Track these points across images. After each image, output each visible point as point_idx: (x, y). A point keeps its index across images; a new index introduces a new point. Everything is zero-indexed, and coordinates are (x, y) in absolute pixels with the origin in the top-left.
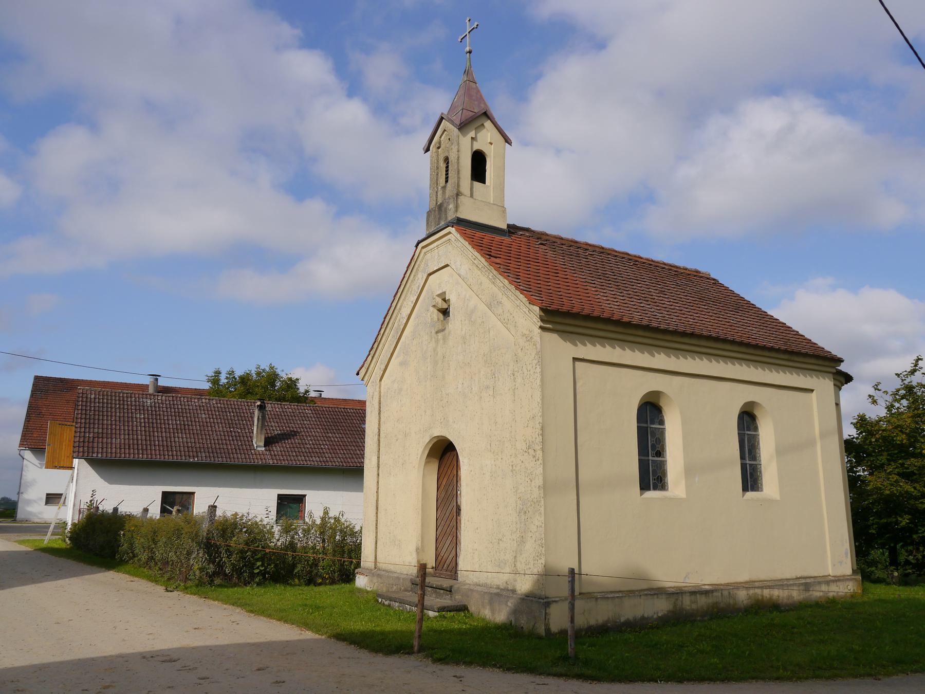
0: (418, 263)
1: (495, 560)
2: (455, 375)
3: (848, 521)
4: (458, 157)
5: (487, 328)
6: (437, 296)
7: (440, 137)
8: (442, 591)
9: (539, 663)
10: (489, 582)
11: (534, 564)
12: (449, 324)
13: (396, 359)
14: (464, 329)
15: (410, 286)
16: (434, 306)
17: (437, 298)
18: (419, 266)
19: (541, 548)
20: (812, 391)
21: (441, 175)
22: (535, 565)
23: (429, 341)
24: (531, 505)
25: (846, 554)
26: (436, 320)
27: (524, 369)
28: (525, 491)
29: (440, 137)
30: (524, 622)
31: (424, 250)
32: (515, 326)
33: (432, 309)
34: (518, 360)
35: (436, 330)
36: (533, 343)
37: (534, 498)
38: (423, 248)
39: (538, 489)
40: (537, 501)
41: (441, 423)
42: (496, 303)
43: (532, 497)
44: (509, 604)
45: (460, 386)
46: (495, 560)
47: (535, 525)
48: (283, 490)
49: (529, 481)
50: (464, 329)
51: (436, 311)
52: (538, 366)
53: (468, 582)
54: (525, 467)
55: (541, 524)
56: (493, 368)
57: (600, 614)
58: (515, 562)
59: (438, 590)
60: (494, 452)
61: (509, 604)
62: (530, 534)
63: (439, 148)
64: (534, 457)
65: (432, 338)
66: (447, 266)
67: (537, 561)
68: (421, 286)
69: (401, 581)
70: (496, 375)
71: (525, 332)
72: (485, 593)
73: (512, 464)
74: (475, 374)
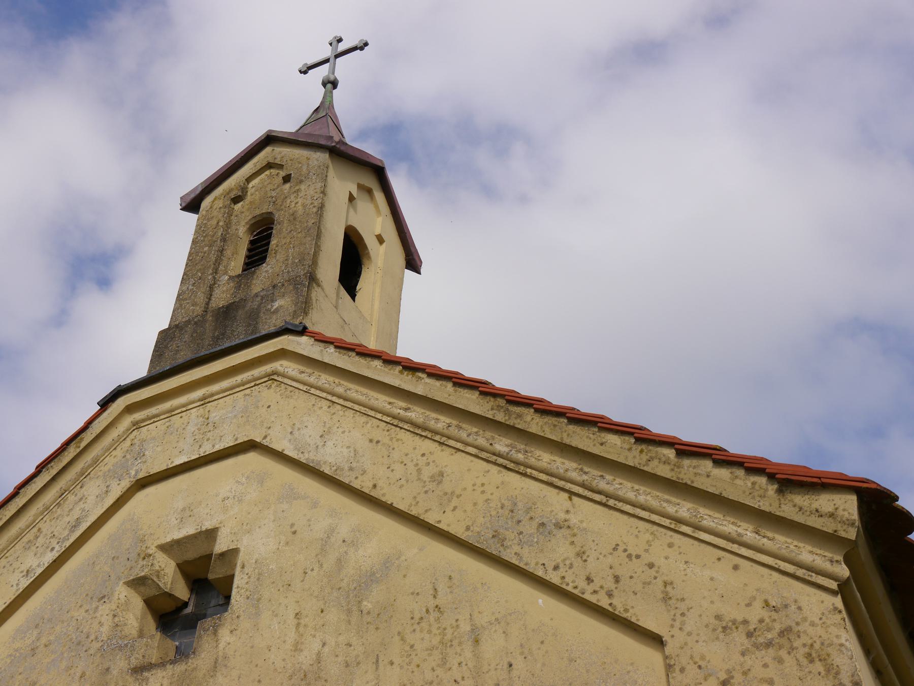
0: (88, 457)
3: (257, 140)
4: (322, 207)
5: (465, 627)
7: (249, 180)
15: (31, 526)
16: (138, 583)
18: (96, 462)
21: (235, 253)
26: (135, 633)
29: (249, 180)
32: (666, 598)
33: (122, 592)
35: (134, 662)
36: (803, 651)
38: (130, 409)
51: (138, 603)
57: (342, 148)
63: (236, 200)
68: (89, 524)
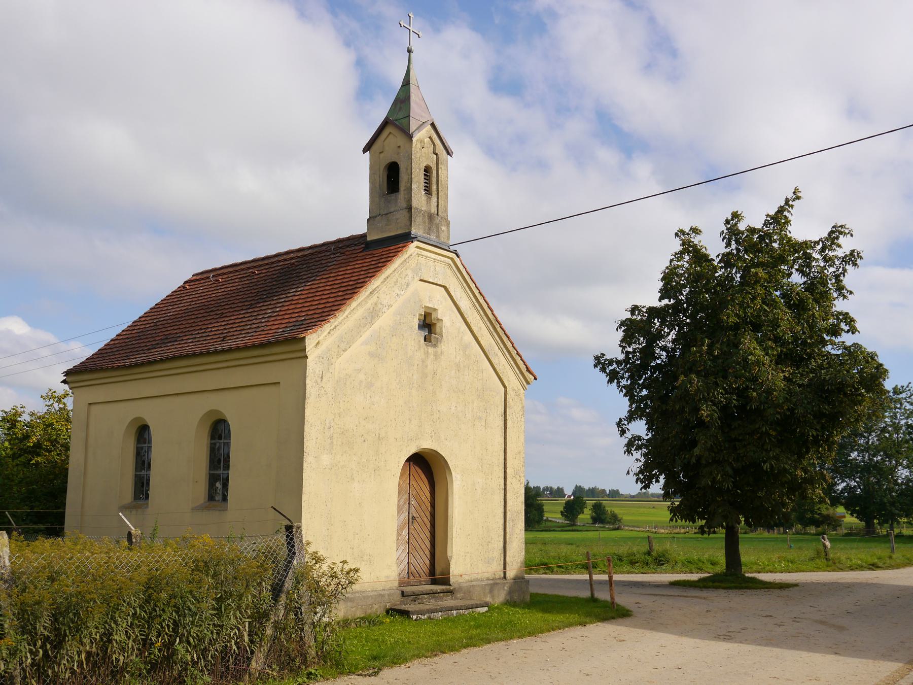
1: (485, 558)
2: (448, 395)
3: (452, 544)
12: (442, 344)
14: (458, 358)
20: (279, 383)
23: (416, 348)
31: (450, 261)
41: (432, 436)
44: (506, 588)
45: (453, 408)
46: (485, 558)
48: (568, 578)
50: (458, 358)
59: (437, 595)
61: (506, 588)
62: (516, 536)
65: (420, 347)
66: (421, 280)
71: (515, 388)
74: (469, 403)
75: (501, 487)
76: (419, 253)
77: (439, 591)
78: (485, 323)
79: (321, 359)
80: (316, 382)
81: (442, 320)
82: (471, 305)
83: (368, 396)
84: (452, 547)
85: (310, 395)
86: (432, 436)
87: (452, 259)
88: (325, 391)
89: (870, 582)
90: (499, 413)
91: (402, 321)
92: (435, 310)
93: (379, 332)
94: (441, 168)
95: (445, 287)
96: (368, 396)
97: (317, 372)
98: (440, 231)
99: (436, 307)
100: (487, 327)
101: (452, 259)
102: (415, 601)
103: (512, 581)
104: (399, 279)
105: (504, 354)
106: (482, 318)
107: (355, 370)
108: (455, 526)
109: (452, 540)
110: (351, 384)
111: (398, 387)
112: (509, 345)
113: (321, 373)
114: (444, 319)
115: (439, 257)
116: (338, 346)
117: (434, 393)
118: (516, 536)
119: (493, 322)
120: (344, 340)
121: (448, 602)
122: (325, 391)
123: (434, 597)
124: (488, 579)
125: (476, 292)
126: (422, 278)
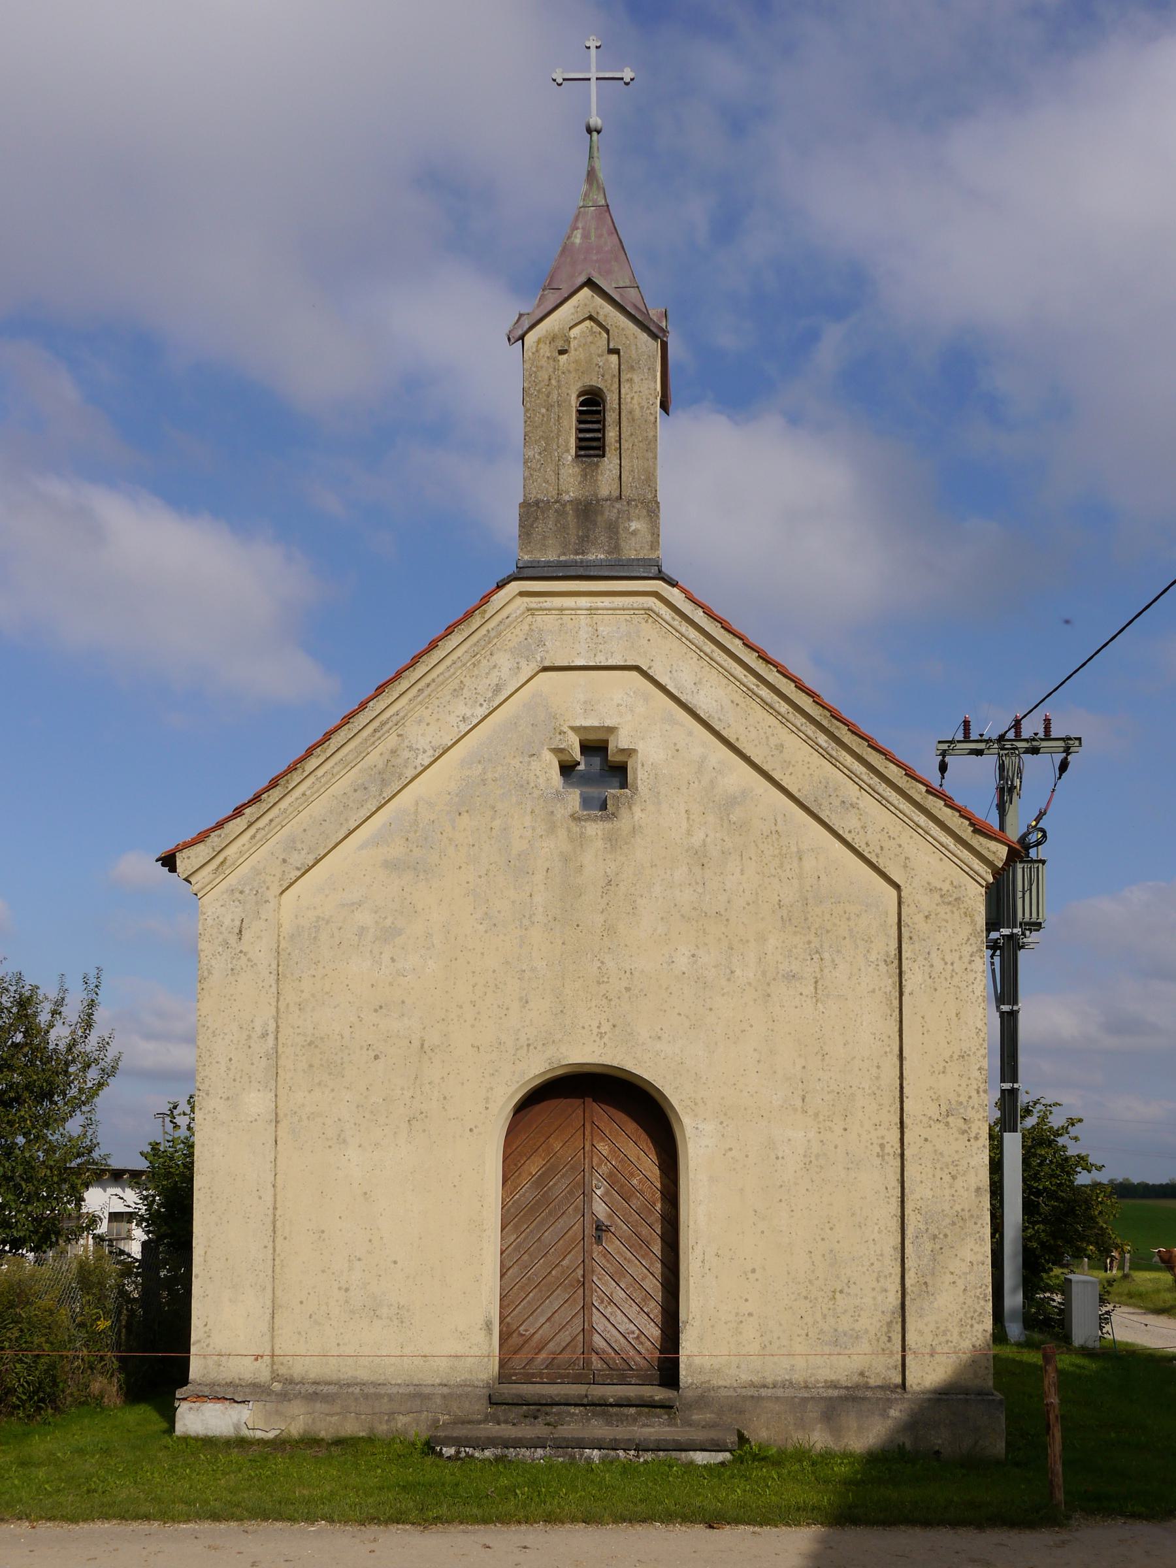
3: (688, 1291)
6: (572, 728)
8: (632, 1410)
9: (295, 1475)
10: (797, 1377)
11: (960, 1334)
12: (636, 809)
13: (362, 847)
17: (570, 733)
19: (982, 1303)
22: (964, 1335)
24: (954, 1224)
25: (488, 1325)
27: (935, 958)
28: (933, 1196)
30: (939, 1440)
31: (651, 602)
32: (905, 867)
34: (915, 938)
37: (963, 1210)
39: (973, 1194)
40: (972, 1216)
41: (601, 1035)
42: (836, 802)
43: (958, 1208)
47: (964, 1260)
49: (947, 1178)
52: (977, 959)
53: (721, 1383)
54: (935, 1151)
55: (981, 1258)
56: (812, 937)
58: (889, 1331)
60: (816, 1115)
62: (948, 1278)
64: (964, 1132)
67: (972, 1326)
69: (438, 1401)
70: (826, 955)
72: (804, 1400)
73: (881, 1141)
75: (888, 1149)
76: (533, 606)
77: (611, 1400)
78: (796, 731)
79: (237, 895)
80: (226, 944)
81: (635, 750)
82: (738, 697)
83: (386, 957)
84: (688, 1300)
85: (210, 973)
86: (601, 1035)
87: (656, 595)
88: (249, 960)
89: (482, 1527)
90: (873, 957)
91: (489, 775)
92: (611, 730)
93: (416, 812)
94: (630, 380)
95: (637, 668)
96: (386, 957)
97: (227, 922)
98: (623, 534)
99: (608, 723)
100: (808, 740)
101: (656, 595)
102: (536, 1418)
103: (484, 1390)
104: (467, 681)
105: (882, 801)
106: (783, 720)
107: (343, 905)
108: (699, 1250)
109: (688, 1280)
110: (332, 936)
111: (482, 928)
112: (893, 772)
113: (238, 923)
114: (640, 747)
115: (607, 601)
116: (284, 861)
117: (610, 929)
118: (948, 1278)
119: (825, 723)
120: (299, 846)
121: (654, 1429)
122: (249, 960)
123: (604, 1414)
124: (834, 1385)
125: (750, 658)
126: (547, 664)
